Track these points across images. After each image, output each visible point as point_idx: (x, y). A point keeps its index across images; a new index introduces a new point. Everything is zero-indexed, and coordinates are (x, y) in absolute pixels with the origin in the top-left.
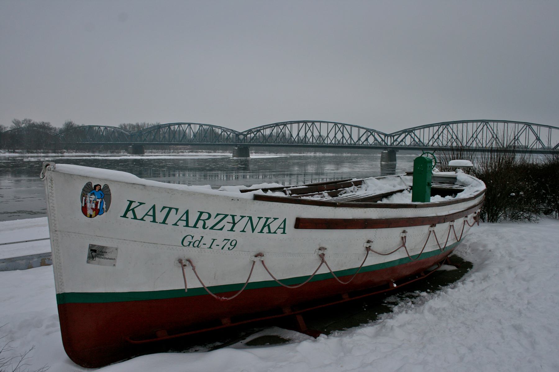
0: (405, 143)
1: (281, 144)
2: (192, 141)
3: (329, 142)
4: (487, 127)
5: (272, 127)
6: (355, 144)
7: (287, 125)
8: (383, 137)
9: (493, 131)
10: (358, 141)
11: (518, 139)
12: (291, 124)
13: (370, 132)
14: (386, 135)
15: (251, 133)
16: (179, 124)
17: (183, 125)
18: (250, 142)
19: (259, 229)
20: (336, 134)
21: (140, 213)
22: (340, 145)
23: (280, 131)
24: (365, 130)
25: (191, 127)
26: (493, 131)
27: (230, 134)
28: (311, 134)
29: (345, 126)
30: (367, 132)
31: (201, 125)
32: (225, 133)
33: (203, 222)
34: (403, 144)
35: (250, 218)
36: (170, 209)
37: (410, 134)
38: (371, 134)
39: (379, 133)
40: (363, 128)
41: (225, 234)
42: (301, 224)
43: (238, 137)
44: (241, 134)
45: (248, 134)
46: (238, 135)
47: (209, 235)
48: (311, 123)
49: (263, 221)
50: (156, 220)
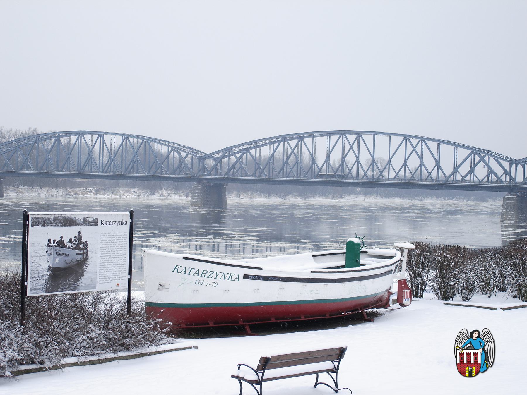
1: (292, 179)
2: (105, 170)
3: (392, 175)
5: (273, 143)
6: (447, 179)
7: (305, 139)
8: (506, 165)
10: (453, 174)
12: (313, 136)
13: (479, 155)
14: (512, 162)
15: (230, 155)
16: (80, 134)
17: (87, 137)
18: (227, 174)
19: (227, 278)
20: (406, 160)
21: (180, 270)
22: (415, 182)
23: (290, 151)
24: (469, 151)
25: (104, 140)
27: (187, 156)
28: (355, 160)
30: (473, 154)
31: (126, 137)
32: (176, 154)
33: (204, 274)
35: (224, 273)
36: (192, 268)
38: (482, 159)
39: (498, 158)
40: (464, 147)
41: (213, 280)
42: (246, 277)
43: (203, 162)
44: (210, 156)
45: (224, 157)
46: (203, 158)
47: (206, 280)
48: (356, 136)
49: (229, 275)
50: (479, 160)
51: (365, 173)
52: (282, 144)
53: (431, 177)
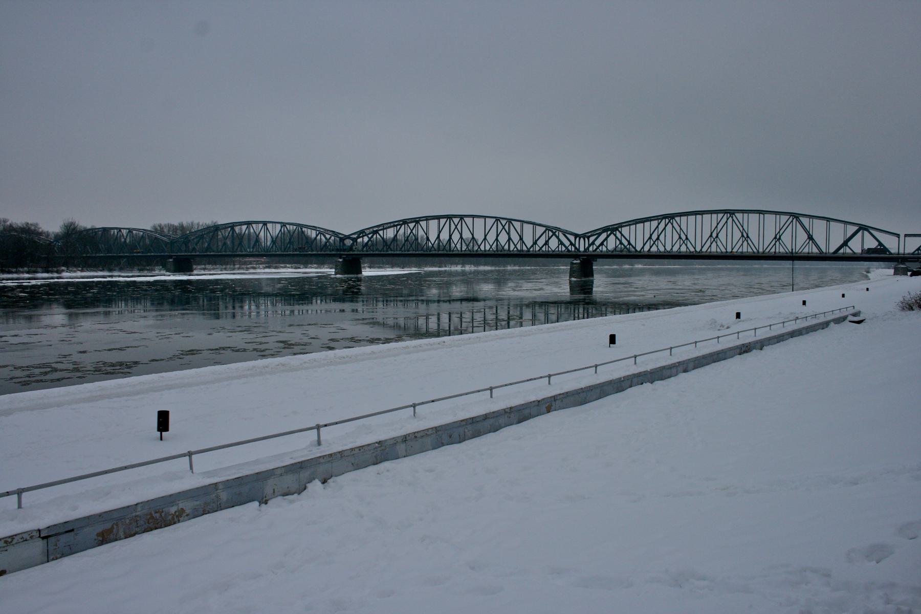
0: (607, 247)
4: (733, 220)
7: (420, 222)
9: (742, 227)
10: (532, 246)
11: (780, 238)
15: (363, 237)
20: (498, 236)
26: (742, 227)
29: (513, 222)
31: (284, 225)
34: (604, 249)
37: (615, 233)
39: (565, 233)
40: (540, 225)
44: (348, 237)
51: (515, 246)
52: (403, 226)
53: (517, 248)
